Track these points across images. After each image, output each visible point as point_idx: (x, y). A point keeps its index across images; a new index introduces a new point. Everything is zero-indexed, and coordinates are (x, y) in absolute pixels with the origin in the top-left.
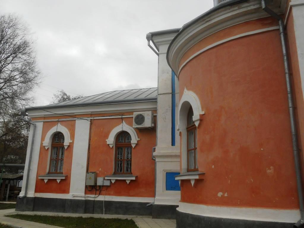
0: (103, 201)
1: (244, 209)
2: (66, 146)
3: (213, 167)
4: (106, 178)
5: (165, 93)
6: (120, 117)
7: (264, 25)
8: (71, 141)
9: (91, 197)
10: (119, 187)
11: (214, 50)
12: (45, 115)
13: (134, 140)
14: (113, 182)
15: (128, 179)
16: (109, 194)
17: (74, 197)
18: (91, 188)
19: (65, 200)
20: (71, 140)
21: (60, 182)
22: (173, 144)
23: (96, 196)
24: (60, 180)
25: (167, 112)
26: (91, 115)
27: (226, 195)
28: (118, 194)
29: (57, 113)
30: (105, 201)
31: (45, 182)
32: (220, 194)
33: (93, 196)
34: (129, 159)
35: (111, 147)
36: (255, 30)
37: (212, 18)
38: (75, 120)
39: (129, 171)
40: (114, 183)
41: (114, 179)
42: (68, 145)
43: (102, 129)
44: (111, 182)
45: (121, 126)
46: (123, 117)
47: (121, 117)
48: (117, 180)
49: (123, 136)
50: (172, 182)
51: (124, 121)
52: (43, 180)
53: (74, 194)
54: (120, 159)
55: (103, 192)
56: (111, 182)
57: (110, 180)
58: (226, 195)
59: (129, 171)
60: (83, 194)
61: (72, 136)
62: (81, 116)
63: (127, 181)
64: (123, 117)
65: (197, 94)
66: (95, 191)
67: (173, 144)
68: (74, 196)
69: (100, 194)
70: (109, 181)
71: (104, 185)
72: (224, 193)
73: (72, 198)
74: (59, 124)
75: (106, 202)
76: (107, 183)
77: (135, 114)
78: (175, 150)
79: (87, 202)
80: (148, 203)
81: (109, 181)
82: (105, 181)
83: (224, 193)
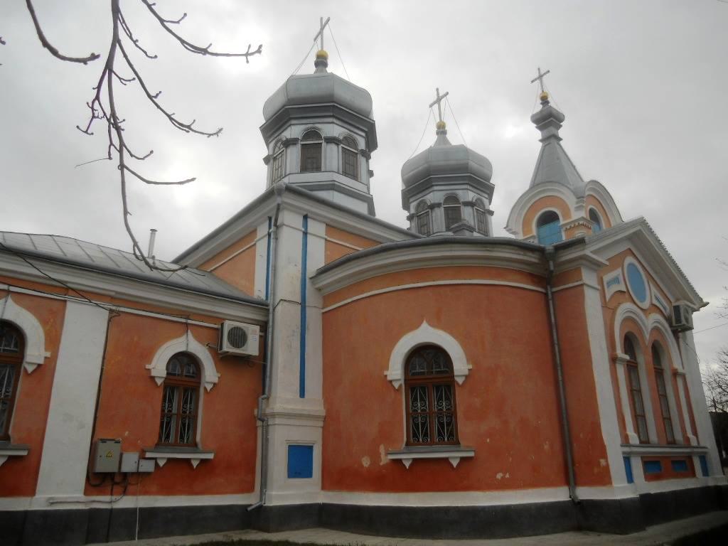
0: (135, 509)
1: (530, 491)
2: (159, 377)
3: (488, 440)
4: (148, 455)
5: (287, 299)
6: (184, 321)
7: (534, 283)
8: (48, 354)
9: (102, 502)
10: (180, 475)
11: (486, 288)
12: (117, 292)
13: (210, 374)
14: (161, 463)
15: (454, 457)
16: (146, 493)
17: (52, 503)
18: (98, 480)
19: (26, 514)
20: (46, 350)
21: (459, 465)
22: (302, 394)
23: (114, 498)
24: (458, 461)
25: (293, 335)
26: (112, 298)
27: (507, 476)
28: (168, 491)
29: (52, 277)
30: (140, 509)
31: (452, 465)
32: (499, 476)
33: (107, 498)
34: (188, 412)
35: (29, 372)
36: (521, 282)
37: (495, 249)
38: (65, 301)
39: (185, 441)
40: (164, 465)
41: (163, 457)
42: (41, 361)
43: (136, 339)
44: (157, 464)
45: (183, 339)
46: (189, 321)
47: (184, 321)
48: (169, 460)
49: (185, 361)
50: (299, 461)
51: (189, 331)
52: (400, 461)
53: (53, 496)
54: (166, 411)
55: (130, 488)
56: (157, 464)
57: (155, 459)
58: (507, 476)
59: (185, 441)
60: (80, 495)
61: (53, 341)
62: (86, 295)
63: (404, 462)
64: (189, 321)
65: (456, 337)
66: (111, 487)
67: (302, 394)
68: (51, 501)
69: (125, 493)
70: (154, 461)
71: (141, 470)
72: (505, 474)
73: (48, 506)
74: (10, 300)
75: (145, 511)
76: (148, 467)
77: (228, 325)
78: (299, 406)
79: (93, 514)
80: (251, 505)
81: (154, 461)
82: (143, 462)
83: (505, 474)
